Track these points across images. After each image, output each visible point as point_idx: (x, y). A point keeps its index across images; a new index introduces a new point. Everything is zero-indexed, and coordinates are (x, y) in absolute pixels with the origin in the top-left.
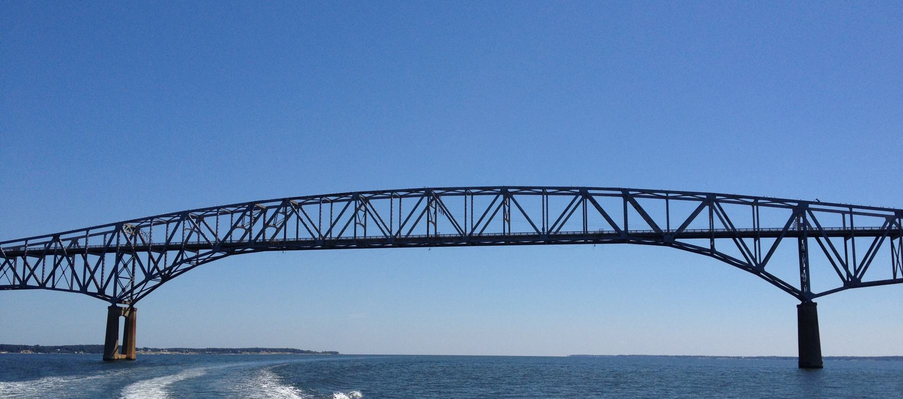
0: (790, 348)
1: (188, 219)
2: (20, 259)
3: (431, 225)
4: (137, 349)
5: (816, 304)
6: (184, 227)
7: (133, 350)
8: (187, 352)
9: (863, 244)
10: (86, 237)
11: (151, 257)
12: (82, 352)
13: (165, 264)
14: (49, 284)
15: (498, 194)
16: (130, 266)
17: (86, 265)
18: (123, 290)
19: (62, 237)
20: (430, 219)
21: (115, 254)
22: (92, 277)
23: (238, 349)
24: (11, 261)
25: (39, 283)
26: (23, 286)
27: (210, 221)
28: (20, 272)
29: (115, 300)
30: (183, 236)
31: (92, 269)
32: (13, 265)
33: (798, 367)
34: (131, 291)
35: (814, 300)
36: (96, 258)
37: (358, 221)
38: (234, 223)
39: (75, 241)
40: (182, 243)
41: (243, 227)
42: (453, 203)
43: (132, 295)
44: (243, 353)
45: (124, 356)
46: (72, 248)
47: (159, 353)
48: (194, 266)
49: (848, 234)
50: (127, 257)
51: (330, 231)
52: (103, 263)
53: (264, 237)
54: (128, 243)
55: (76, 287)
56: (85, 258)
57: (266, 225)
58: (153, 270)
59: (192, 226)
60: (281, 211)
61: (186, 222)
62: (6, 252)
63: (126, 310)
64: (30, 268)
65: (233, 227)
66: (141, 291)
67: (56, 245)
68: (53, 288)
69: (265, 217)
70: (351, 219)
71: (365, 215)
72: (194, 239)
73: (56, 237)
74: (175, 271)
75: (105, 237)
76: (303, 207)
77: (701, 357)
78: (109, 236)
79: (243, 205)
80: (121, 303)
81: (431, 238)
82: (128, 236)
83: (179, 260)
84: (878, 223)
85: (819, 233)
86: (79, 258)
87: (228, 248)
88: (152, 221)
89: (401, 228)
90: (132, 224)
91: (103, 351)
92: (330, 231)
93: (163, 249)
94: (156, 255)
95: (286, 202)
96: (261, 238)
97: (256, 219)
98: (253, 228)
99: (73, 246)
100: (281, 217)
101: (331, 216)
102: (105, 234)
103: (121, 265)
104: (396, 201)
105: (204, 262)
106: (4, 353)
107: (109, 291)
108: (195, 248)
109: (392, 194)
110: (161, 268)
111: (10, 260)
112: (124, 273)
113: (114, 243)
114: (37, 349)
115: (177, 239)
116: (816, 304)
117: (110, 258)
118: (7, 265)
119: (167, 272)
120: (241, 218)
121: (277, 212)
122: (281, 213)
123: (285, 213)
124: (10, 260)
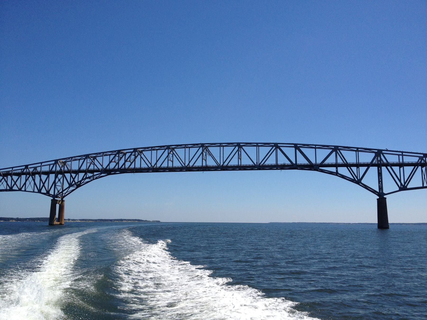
0: (374, 219)
1: (89, 158)
2: (9, 177)
3: (204, 161)
4: (65, 220)
5: (386, 198)
6: (87, 162)
7: (63, 220)
8: (89, 221)
9: (408, 170)
10: (41, 166)
11: (71, 176)
12: (39, 221)
13: (78, 179)
14: (23, 189)
15: (235, 146)
16: (61, 180)
17: (41, 180)
18: (58, 191)
19: (29, 167)
20: (203, 158)
21: (54, 175)
22: (44, 186)
24: (5, 178)
25: (18, 188)
26: (11, 189)
27: (100, 159)
28: (9, 183)
29: (54, 196)
30: (87, 166)
31: (44, 182)
32: (6, 180)
33: (377, 228)
34: (62, 192)
36: (17, 177)
37: (169, 159)
38: (111, 160)
39: (35, 168)
40: (86, 169)
41: (115, 162)
42: (180, 152)
43: (62, 194)
44: (115, 222)
45: (59, 223)
46: (34, 172)
47: (75, 221)
48: (92, 180)
49: (401, 165)
50: (60, 176)
51: (156, 164)
52: (49, 179)
53: (125, 167)
54: (61, 169)
55: (36, 190)
56: (40, 177)
57: (126, 161)
58: (72, 182)
59: (91, 161)
60: (133, 154)
61: (88, 159)
62: (3, 174)
63: (59, 201)
64: (14, 181)
65: (110, 162)
66: (67, 192)
67: (26, 170)
68: (25, 191)
69: (125, 157)
70: (166, 158)
71: (173, 156)
72: (92, 167)
73: (27, 167)
74: (83, 183)
75: (50, 167)
76: (143, 152)
77: (332, 223)
78: (51, 166)
79: (115, 151)
80: (57, 198)
81: (204, 167)
82: (61, 166)
83: (85, 177)
84: (415, 160)
85: (387, 165)
86: (37, 176)
87: (108, 172)
88: (72, 159)
89: (190, 162)
90: (63, 160)
91: (49, 220)
92: (156, 164)
93: (77, 172)
94: (74, 175)
95: (135, 150)
96: (123, 167)
97: (121, 158)
98: (119, 162)
99: (34, 170)
100: (133, 157)
101: (157, 157)
102: (50, 165)
103: (57, 180)
104: (187, 149)
105: (97, 178)
106: (2, 221)
107: (52, 192)
108: (92, 172)
109: (185, 146)
111: (5, 177)
112: (59, 184)
113: (54, 169)
114: (17, 219)
115: (84, 168)
116: (386, 198)
117: (52, 176)
118: (3, 180)
119: (79, 183)
121: (131, 155)
122: (133, 155)
123: (135, 155)
124: (5, 177)
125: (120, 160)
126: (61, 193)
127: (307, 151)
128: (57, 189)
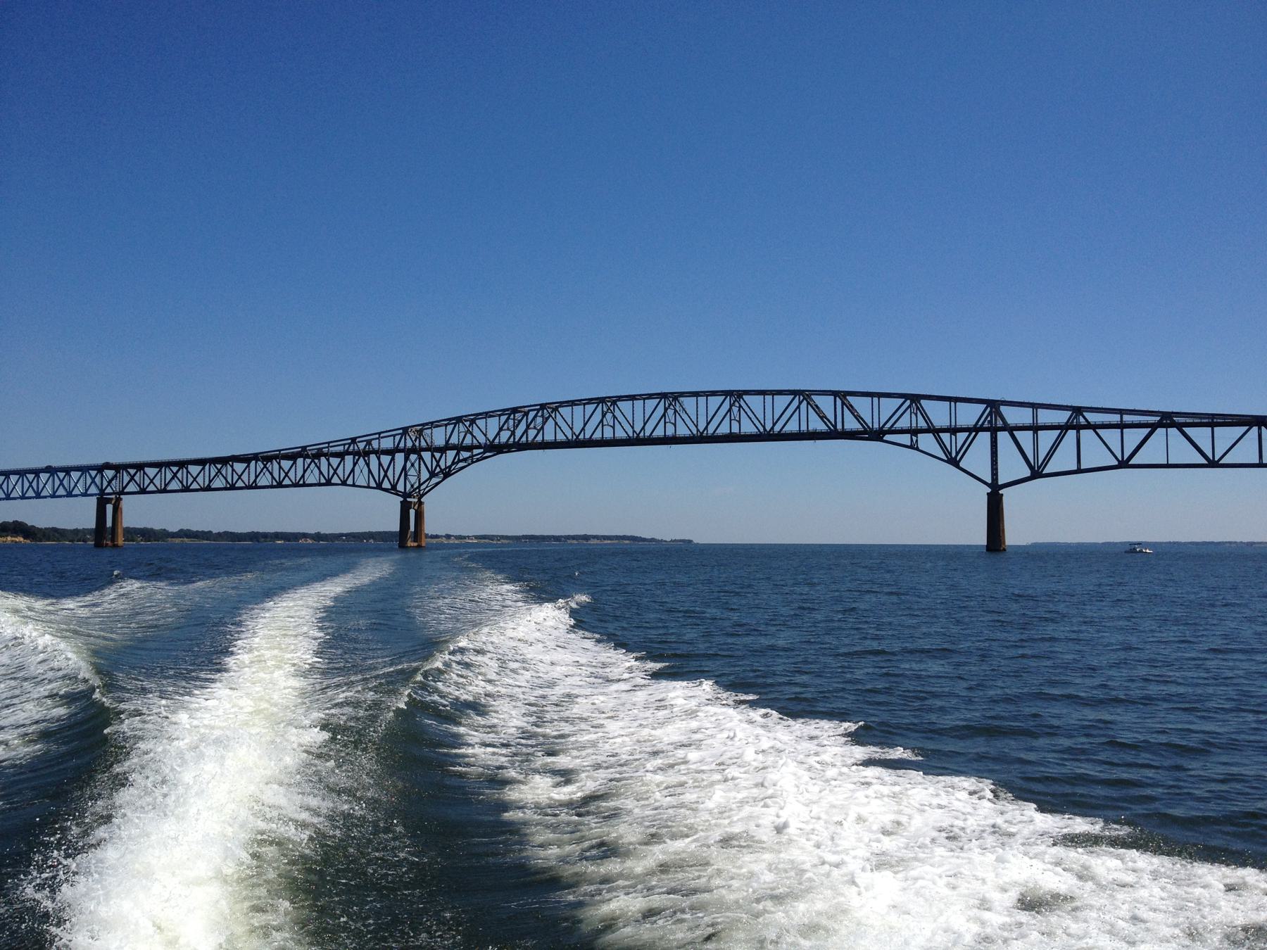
0: (980, 537)
4: (427, 536)
12: (372, 541)
14: (350, 482)
16: (416, 465)
17: (380, 464)
18: (412, 486)
19: (358, 440)
21: (403, 454)
22: (386, 475)
23: (562, 536)
24: (316, 461)
26: (329, 483)
27: (481, 423)
29: (405, 495)
34: (419, 487)
35: (1001, 492)
36: (291, 462)
41: (508, 429)
42: (754, 402)
43: (420, 491)
44: (569, 541)
45: (416, 544)
47: (463, 541)
48: (469, 465)
49: (1035, 428)
50: (413, 457)
51: (706, 428)
53: (527, 438)
54: (414, 445)
55: (373, 484)
57: (528, 427)
58: (436, 468)
60: (540, 414)
68: (354, 485)
69: (527, 419)
70: (588, 420)
71: (739, 410)
72: (468, 441)
73: (354, 440)
77: (1230, 543)
78: (398, 438)
79: (507, 410)
85: (1089, 426)
86: (373, 457)
87: (496, 448)
88: (433, 425)
89: (774, 424)
91: (398, 538)
92: (706, 428)
93: (443, 450)
94: (437, 455)
95: (543, 406)
96: (512, 440)
97: (520, 421)
100: (539, 420)
102: (394, 436)
103: (409, 464)
105: (478, 460)
107: (400, 487)
108: (470, 448)
110: (443, 467)
112: (412, 472)
113: (402, 445)
114: (318, 537)
115: (454, 440)
117: (400, 457)
118: (313, 464)
120: (506, 421)
121: (536, 416)
123: (542, 416)
125: (517, 426)
126: (416, 489)
127: (862, 405)
128: (410, 482)
